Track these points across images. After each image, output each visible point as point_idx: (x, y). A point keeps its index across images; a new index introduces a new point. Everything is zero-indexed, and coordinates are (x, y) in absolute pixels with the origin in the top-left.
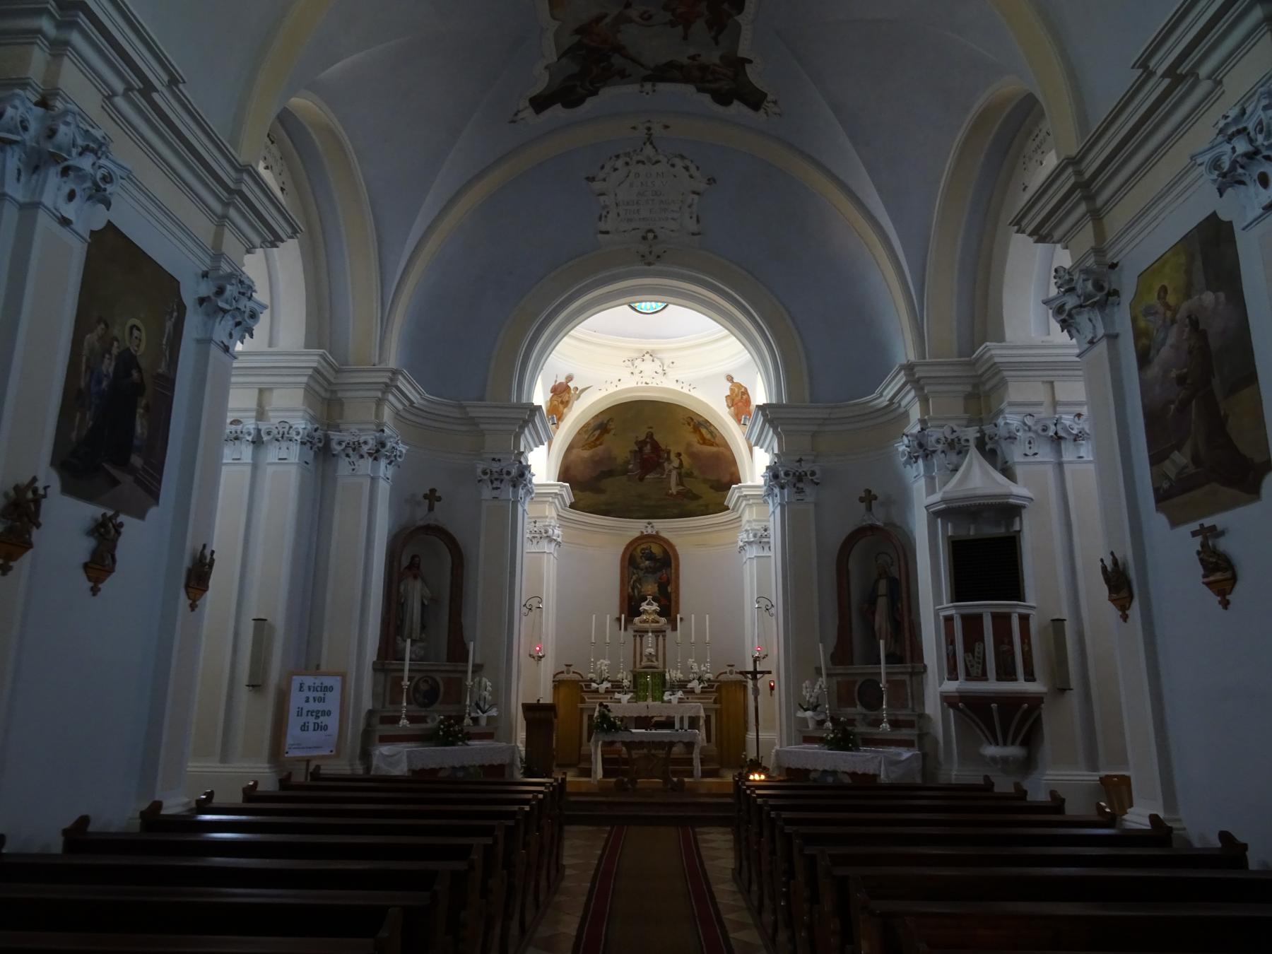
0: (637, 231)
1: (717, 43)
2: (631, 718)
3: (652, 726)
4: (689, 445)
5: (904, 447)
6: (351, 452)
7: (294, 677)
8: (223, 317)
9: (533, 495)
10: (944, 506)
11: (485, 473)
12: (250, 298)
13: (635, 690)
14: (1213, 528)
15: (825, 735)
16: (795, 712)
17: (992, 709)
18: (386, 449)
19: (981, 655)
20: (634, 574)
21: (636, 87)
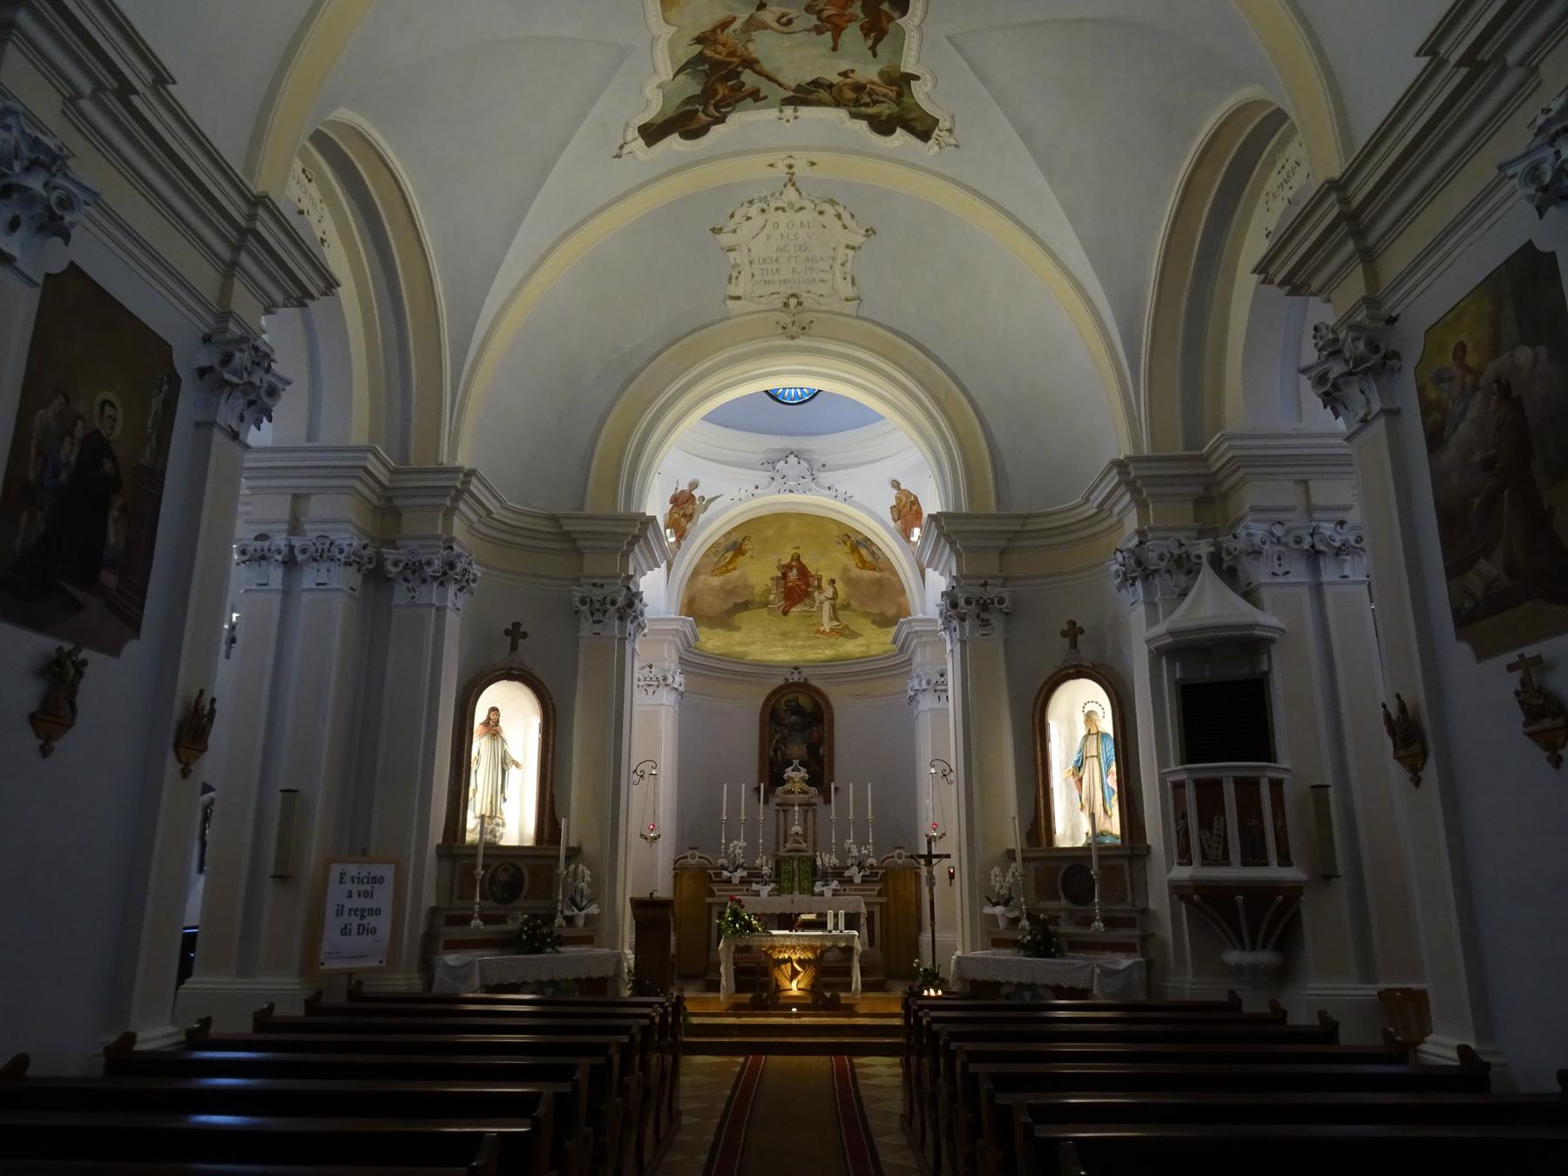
0: (775, 296)
1: (875, 55)
2: (772, 915)
3: (798, 926)
4: (845, 570)
5: (1118, 566)
6: (410, 576)
7: (333, 865)
8: (230, 394)
9: (646, 631)
10: (1171, 640)
11: (583, 602)
12: (268, 370)
13: (778, 879)
14: (1538, 659)
15: (1020, 937)
16: (982, 908)
17: (1236, 902)
18: (455, 571)
19: (1222, 833)
20: (776, 732)
21: (773, 113)
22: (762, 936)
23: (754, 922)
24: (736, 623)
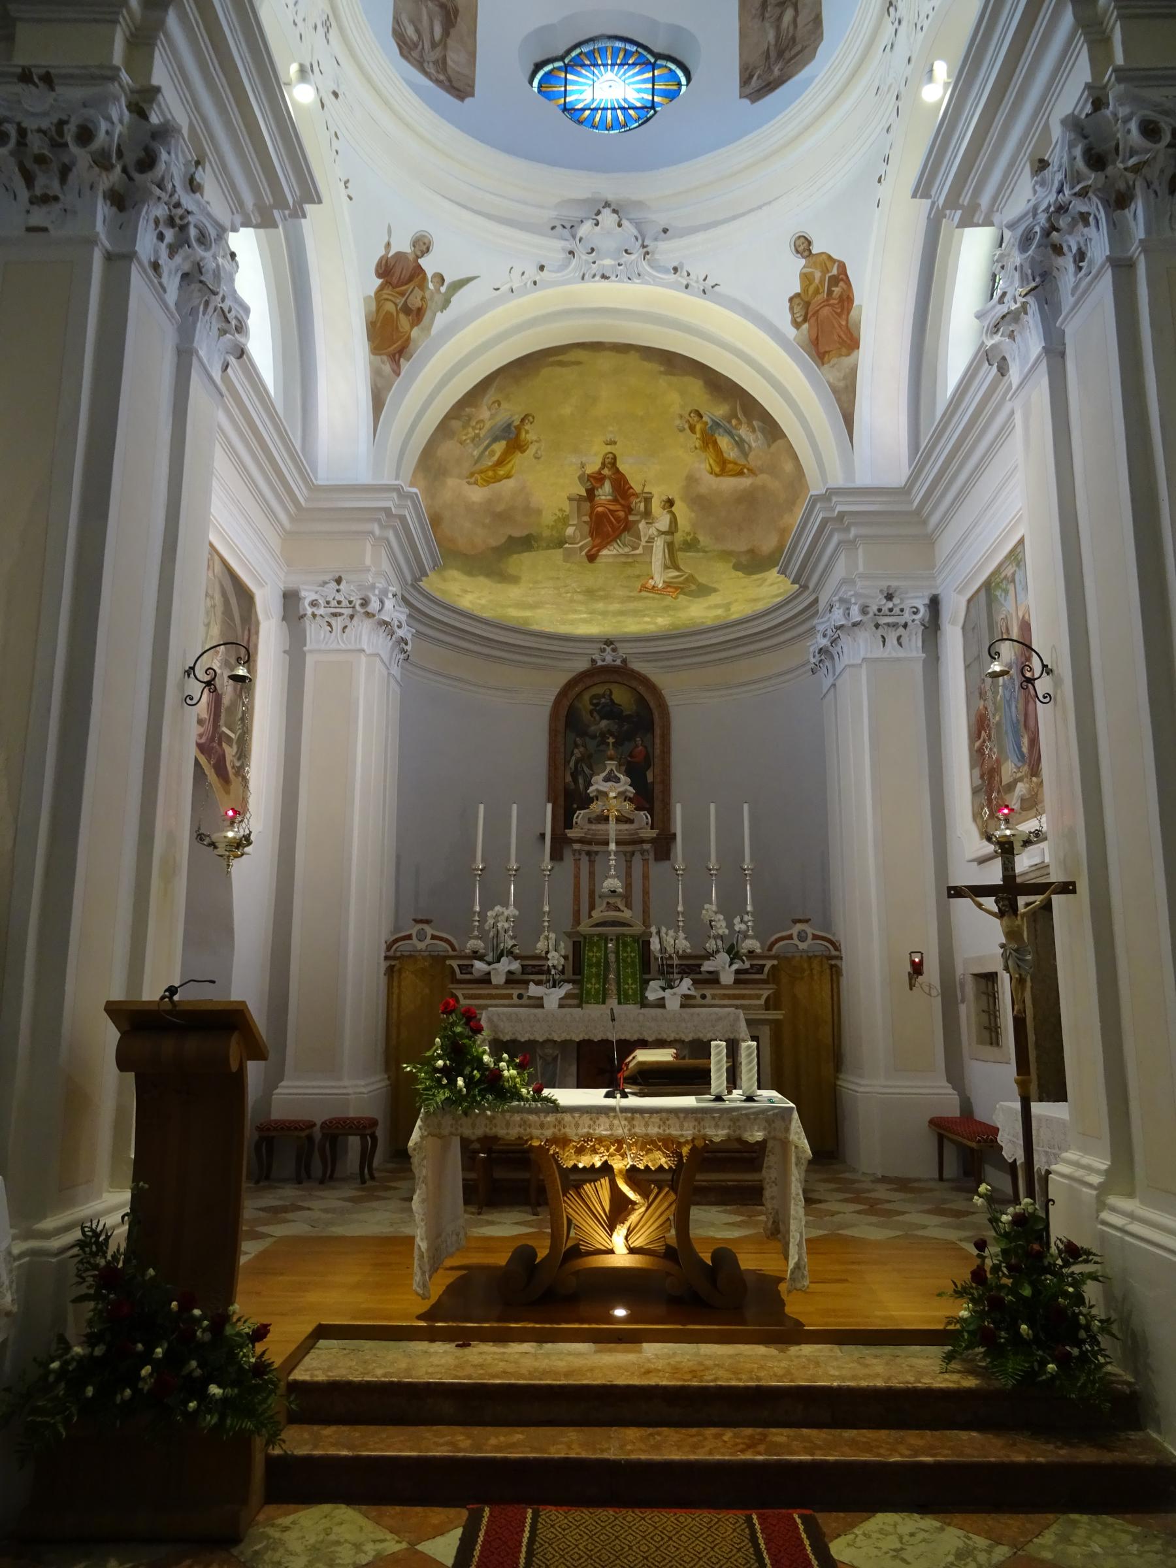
2: (565, 1044)
4: (691, 480)
13: (578, 977)
20: (576, 746)
22: (531, 1111)
23: (509, 1073)
24: (512, 571)
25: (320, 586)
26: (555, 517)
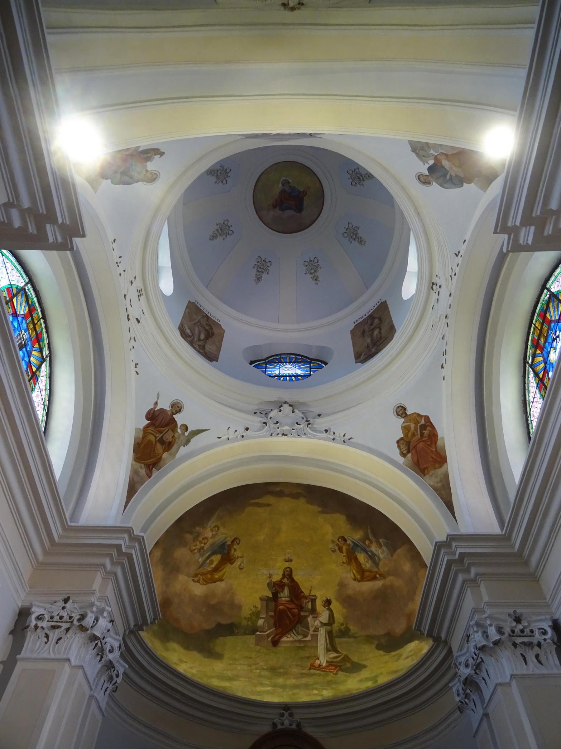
4: (342, 585)
24: (218, 649)
25: (52, 604)
26: (251, 612)
